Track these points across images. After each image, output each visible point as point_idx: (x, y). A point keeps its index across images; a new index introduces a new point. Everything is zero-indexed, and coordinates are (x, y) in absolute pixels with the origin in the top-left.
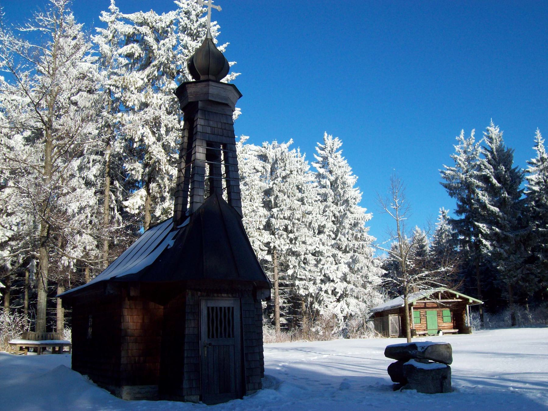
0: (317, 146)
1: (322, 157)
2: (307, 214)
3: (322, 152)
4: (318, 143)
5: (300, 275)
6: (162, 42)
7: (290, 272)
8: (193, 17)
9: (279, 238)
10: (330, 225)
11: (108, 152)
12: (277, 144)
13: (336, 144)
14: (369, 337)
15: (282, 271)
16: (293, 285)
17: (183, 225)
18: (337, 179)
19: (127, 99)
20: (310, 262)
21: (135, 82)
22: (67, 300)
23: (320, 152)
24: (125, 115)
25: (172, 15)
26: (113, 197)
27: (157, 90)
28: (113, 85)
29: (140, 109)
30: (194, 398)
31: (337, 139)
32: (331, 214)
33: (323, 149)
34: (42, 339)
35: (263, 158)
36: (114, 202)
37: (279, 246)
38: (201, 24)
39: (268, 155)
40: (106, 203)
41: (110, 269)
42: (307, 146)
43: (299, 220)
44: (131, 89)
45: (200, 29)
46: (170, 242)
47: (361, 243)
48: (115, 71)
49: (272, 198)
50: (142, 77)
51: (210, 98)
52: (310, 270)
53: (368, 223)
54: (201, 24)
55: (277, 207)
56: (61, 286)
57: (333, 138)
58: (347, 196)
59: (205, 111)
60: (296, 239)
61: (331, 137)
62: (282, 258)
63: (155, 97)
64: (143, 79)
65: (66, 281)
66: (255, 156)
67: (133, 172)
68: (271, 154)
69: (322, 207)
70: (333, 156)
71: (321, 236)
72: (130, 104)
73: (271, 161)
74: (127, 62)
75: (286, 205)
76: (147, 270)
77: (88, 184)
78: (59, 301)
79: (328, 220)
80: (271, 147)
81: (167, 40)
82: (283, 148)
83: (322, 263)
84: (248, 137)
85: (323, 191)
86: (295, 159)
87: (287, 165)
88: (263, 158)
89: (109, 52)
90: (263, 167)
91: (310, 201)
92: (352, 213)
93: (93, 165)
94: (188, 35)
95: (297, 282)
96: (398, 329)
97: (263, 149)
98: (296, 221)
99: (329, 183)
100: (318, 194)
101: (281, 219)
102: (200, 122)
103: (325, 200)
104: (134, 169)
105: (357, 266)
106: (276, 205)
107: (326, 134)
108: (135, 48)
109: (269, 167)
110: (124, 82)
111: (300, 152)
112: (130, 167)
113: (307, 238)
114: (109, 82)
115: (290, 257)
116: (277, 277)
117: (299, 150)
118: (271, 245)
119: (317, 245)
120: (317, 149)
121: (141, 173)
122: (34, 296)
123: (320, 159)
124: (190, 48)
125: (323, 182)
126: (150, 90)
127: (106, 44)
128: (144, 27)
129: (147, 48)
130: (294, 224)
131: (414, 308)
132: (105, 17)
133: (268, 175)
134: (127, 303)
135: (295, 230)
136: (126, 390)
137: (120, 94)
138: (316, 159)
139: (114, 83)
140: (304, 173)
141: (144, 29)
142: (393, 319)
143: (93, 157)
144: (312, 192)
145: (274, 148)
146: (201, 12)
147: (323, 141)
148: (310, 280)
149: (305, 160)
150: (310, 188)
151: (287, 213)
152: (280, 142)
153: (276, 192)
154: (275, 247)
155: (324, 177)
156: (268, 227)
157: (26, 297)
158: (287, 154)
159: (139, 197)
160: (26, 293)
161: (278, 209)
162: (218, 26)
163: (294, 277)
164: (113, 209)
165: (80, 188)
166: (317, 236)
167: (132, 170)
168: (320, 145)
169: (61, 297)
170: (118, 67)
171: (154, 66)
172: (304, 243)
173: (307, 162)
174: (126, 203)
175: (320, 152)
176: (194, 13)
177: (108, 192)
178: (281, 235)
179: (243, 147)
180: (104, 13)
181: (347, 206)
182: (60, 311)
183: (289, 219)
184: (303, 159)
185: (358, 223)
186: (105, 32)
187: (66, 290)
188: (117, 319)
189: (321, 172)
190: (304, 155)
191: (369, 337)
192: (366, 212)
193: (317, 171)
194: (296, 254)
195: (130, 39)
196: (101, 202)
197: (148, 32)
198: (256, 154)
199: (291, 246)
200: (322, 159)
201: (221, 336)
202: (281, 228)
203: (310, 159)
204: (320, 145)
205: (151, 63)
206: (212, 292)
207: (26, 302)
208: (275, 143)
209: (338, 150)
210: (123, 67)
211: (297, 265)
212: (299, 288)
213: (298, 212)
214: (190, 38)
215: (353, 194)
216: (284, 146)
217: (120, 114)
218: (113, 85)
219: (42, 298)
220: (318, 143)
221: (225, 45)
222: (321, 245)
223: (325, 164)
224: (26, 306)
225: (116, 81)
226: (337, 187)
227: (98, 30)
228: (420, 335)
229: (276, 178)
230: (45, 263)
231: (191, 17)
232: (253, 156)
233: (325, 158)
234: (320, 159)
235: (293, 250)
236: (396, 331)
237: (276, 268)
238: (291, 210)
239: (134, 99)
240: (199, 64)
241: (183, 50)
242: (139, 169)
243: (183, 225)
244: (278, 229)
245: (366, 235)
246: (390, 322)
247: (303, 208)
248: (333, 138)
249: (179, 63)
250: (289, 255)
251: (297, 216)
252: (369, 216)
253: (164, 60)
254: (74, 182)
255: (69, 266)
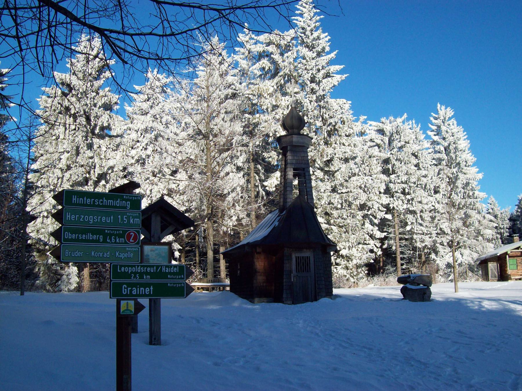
0: (432, 116)
1: (436, 126)
2: (423, 176)
3: (436, 121)
4: (432, 114)
5: (417, 230)
6: (286, 55)
7: (408, 228)
8: (308, 33)
9: (398, 200)
10: (443, 186)
11: (251, 145)
12: (393, 119)
13: (448, 113)
14: (471, 281)
15: (402, 227)
16: (412, 239)
17: (283, 214)
18: (449, 145)
19: (262, 103)
20: (425, 219)
21: (268, 90)
22: (225, 254)
23: (434, 121)
24: (262, 116)
25: (292, 32)
26: (257, 178)
27: (285, 94)
28: (251, 94)
29: (273, 110)
30: (289, 302)
31: (449, 109)
32: (445, 176)
33: (436, 119)
34: (214, 282)
35: (381, 132)
36: (258, 181)
37: (397, 207)
38: (314, 38)
39: (385, 129)
40: (252, 182)
41: (256, 232)
42: (422, 117)
43: (415, 183)
44: (265, 96)
45: (314, 42)
46: (277, 223)
47: (473, 200)
48: (252, 81)
49: (390, 166)
50: (272, 85)
51: (294, 144)
52: (426, 226)
53: (480, 182)
54: (314, 38)
55: (395, 173)
56: (222, 246)
57: (446, 108)
58: (459, 159)
59: (291, 151)
60: (412, 199)
61: (443, 107)
62: (402, 216)
63: (283, 100)
64: (273, 87)
65: (225, 243)
66: (374, 131)
67: (270, 159)
68: (388, 128)
69: (437, 171)
70: (446, 124)
71: (437, 195)
72: (264, 107)
73: (388, 134)
74: (261, 73)
75: (402, 171)
76: (265, 238)
77: (239, 169)
78: (222, 256)
79: (442, 181)
80: (388, 121)
81: (290, 53)
82: (398, 122)
83: (437, 219)
84: (366, 117)
85: (438, 156)
86: (409, 130)
87: (402, 137)
88: (381, 132)
89: (246, 66)
90: (382, 140)
91: (425, 165)
92: (465, 174)
93: (241, 155)
94: (305, 47)
95: (415, 236)
96: (497, 275)
97: (381, 124)
98: (412, 185)
99: (442, 149)
100: (434, 159)
101: (398, 183)
102: (289, 156)
103: (440, 164)
104: (271, 157)
105: (469, 220)
106: (394, 172)
107: (439, 105)
108: (265, 63)
109: (386, 140)
110: (259, 91)
111: (415, 123)
112: (267, 155)
113: (423, 198)
114: (248, 92)
115: (408, 215)
116: (397, 233)
117: (414, 122)
118: (390, 206)
119: (433, 204)
120: (432, 119)
121: (276, 159)
122: (204, 254)
123: (434, 128)
124: (307, 58)
125: (437, 148)
126: (279, 95)
127: (244, 59)
128: (271, 46)
129: (273, 62)
130: (410, 187)
131: (509, 257)
132: (242, 38)
133: (386, 146)
134: (256, 256)
135: (412, 192)
136: (256, 300)
137: (256, 101)
138: (431, 128)
139: (252, 92)
140: (419, 142)
141: (271, 49)
142: (492, 266)
143: (240, 148)
144: (427, 158)
145: (390, 123)
146: (315, 27)
147: (437, 112)
148: (427, 234)
149: (420, 130)
150: (424, 154)
151: (404, 178)
152: (395, 117)
153: (393, 161)
154: (393, 208)
155: (438, 144)
156: (388, 191)
157: (197, 255)
158: (402, 127)
159: (275, 178)
160: (197, 252)
161: (395, 175)
162: (329, 37)
163: (411, 232)
164: (258, 186)
165: (233, 172)
166: (434, 196)
167: (269, 158)
168: (434, 115)
169: (223, 253)
170: (254, 78)
171: (280, 76)
172: (420, 202)
173: (421, 132)
174: (265, 184)
175: (434, 121)
176: (309, 29)
177: (253, 174)
178: (399, 197)
179: (362, 126)
180: (240, 35)
181: (459, 168)
182: (223, 264)
183: (406, 183)
184: (418, 129)
185: (469, 183)
186: (242, 50)
187: (226, 249)
188: (252, 264)
189: (435, 140)
190: (420, 126)
191: (471, 281)
192: (478, 172)
193: (432, 139)
194: (413, 212)
195: (261, 56)
196: (248, 181)
197: (274, 51)
198: (376, 128)
199: (409, 206)
200: (436, 128)
201: (303, 271)
202: (399, 191)
203: (425, 129)
204: (434, 115)
205: (278, 73)
206: (300, 249)
207: (197, 259)
208: (392, 118)
209: (450, 119)
210: (257, 77)
211: (414, 221)
212: (416, 241)
213: (413, 177)
214: (307, 49)
215: (467, 157)
216: (399, 120)
217: (258, 115)
218: (251, 94)
219: (210, 254)
220: (432, 114)
221: (335, 53)
222: (437, 204)
223: (438, 132)
224: (198, 261)
225: (253, 91)
226: (450, 152)
227: (237, 49)
228: (516, 279)
229: (393, 149)
230: (211, 232)
231: (307, 33)
232: (372, 131)
233: (439, 127)
234: (434, 128)
235: (410, 209)
236: (495, 277)
237: (396, 225)
238: (408, 175)
239: (267, 103)
240: (289, 122)
241: (302, 61)
242: (274, 156)
243: (283, 214)
244: (397, 192)
245: (477, 193)
246: (489, 269)
247: (419, 172)
248: (446, 108)
249: (299, 71)
250: (407, 213)
251: (413, 180)
252: (480, 176)
253: (287, 71)
254: (228, 168)
255: (227, 231)
